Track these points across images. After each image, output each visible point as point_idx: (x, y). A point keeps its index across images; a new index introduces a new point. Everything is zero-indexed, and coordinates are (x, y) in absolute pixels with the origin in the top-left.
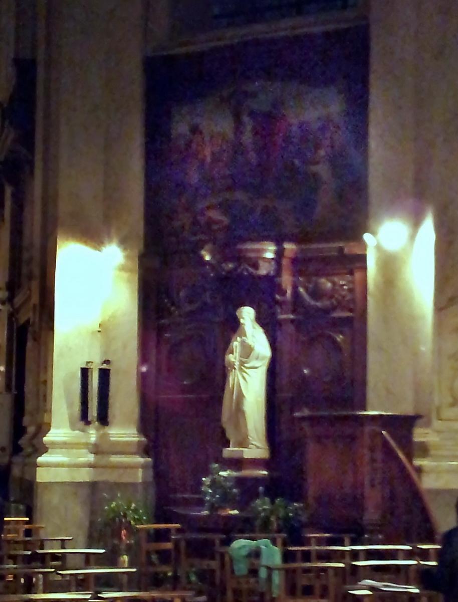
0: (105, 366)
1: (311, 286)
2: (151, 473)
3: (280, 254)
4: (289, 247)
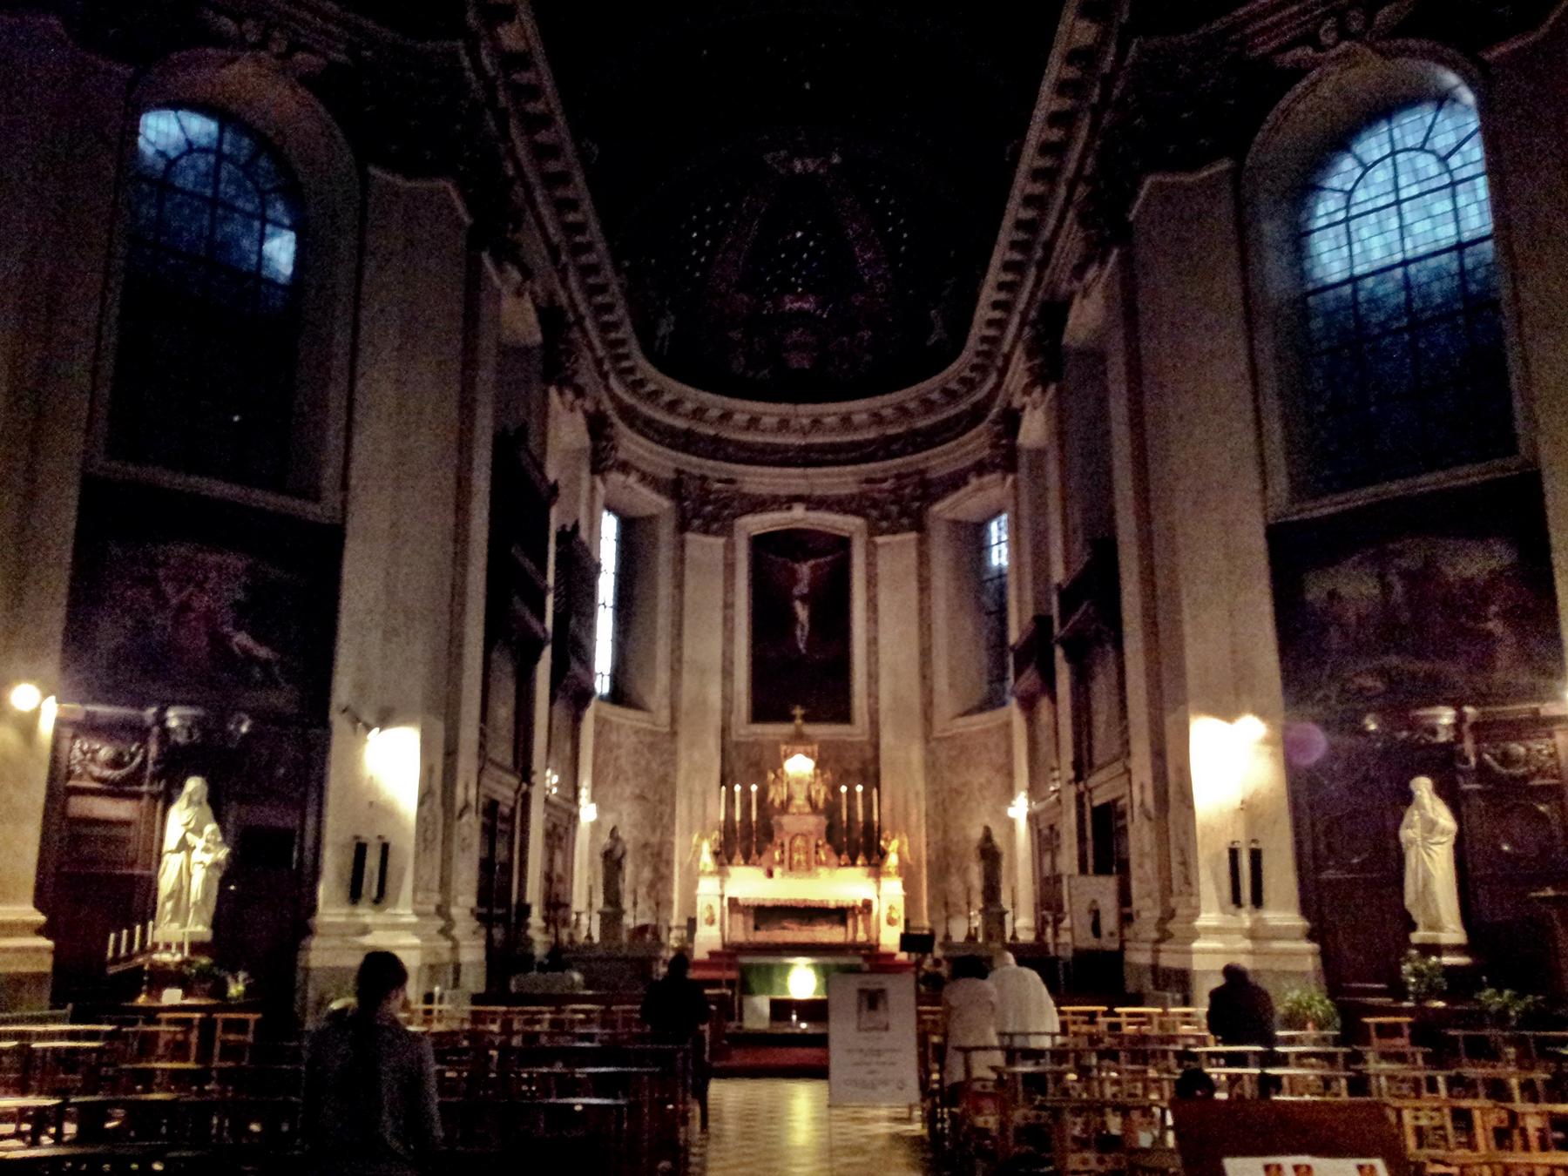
0: (1254, 846)
1: (1498, 752)
2: (1318, 960)
3: (1460, 718)
4: (1469, 710)
